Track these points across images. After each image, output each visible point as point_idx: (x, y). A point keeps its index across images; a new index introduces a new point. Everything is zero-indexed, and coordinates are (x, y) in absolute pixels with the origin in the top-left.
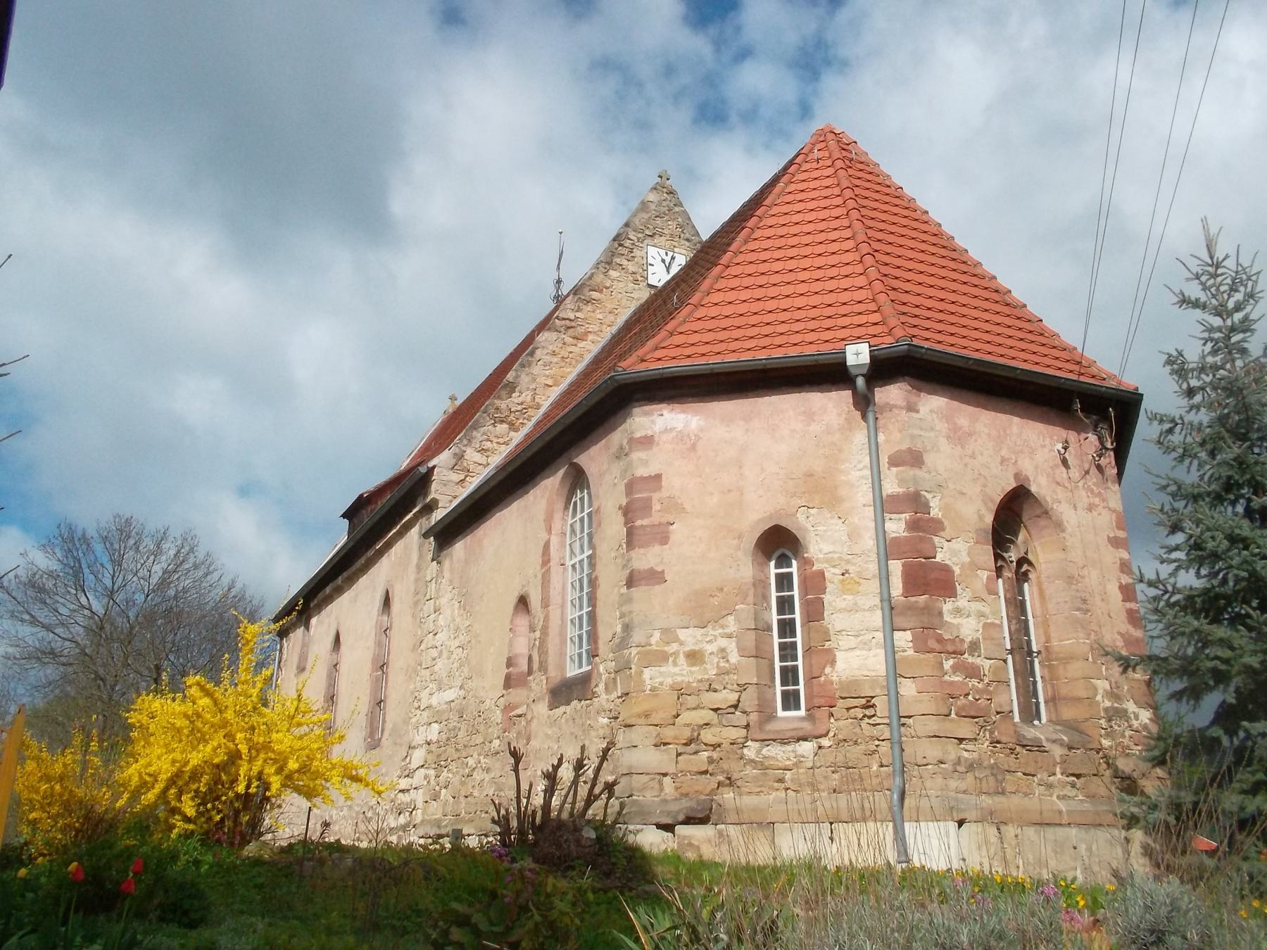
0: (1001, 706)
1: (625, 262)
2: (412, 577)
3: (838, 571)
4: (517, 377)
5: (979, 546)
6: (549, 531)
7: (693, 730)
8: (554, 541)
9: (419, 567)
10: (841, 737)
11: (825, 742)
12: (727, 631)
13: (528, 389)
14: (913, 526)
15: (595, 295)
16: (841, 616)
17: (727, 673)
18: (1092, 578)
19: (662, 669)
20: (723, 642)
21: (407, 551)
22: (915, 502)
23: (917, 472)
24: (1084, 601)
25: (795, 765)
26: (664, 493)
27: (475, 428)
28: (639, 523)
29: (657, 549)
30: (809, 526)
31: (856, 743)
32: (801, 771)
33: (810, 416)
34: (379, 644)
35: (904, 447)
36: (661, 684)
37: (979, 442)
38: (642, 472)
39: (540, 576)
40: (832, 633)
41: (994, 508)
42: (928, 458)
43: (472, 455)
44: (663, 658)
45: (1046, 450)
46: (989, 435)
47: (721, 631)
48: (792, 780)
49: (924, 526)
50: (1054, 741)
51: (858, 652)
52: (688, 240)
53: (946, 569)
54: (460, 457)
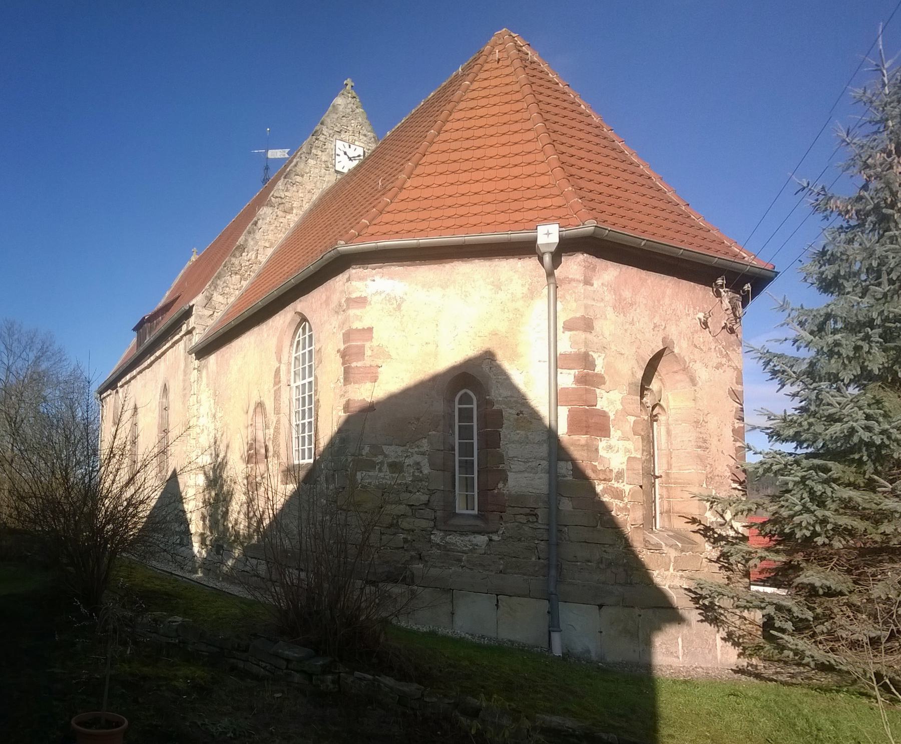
0: (635, 520)
1: (320, 153)
2: (181, 378)
3: (514, 412)
4: (246, 240)
5: (630, 397)
6: (280, 362)
7: (393, 518)
8: (283, 368)
9: (185, 373)
10: (508, 535)
11: (495, 538)
12: (422, 450)
13: (253, 250)
14: (582, 380)
15: (298, 179)
16: (513, 446)
17: (421, 480)
18: (713, 423)
19: (370, 474)
20: (418, 458)
21: (175, 356)
22: (586, 360)
23: (588, 335)
24: (705, 441)
25: (471, 550)
26: (375, 343)
27: (218, 277)
28: (354, 365)
29: (369, 385)
30: (491, 375)
31: (519, 540)
32: (475, 555)
33: (498, 287)
34: (162, 417)
35: (578, 315)
36: (370, 483)
37: (638, 311)
38: (357, 325)
39: (272, 391)
40: (505, 458)
41: (644, 367)
42: (597, 325)
43: (217, 298)
44: (372, 465)
45: (690, 318)
46: (646, 305)
47: (416, 449)
48: (468, 561)
49: (589, 380)
50: (671, 546)
51: (526, 475)
52: (365, 135)
53: (604, 415)
54: (209, 299)
